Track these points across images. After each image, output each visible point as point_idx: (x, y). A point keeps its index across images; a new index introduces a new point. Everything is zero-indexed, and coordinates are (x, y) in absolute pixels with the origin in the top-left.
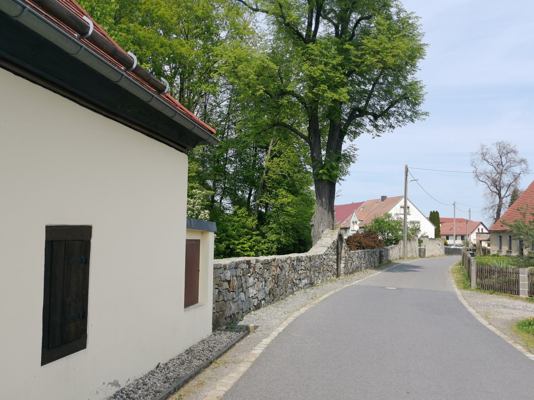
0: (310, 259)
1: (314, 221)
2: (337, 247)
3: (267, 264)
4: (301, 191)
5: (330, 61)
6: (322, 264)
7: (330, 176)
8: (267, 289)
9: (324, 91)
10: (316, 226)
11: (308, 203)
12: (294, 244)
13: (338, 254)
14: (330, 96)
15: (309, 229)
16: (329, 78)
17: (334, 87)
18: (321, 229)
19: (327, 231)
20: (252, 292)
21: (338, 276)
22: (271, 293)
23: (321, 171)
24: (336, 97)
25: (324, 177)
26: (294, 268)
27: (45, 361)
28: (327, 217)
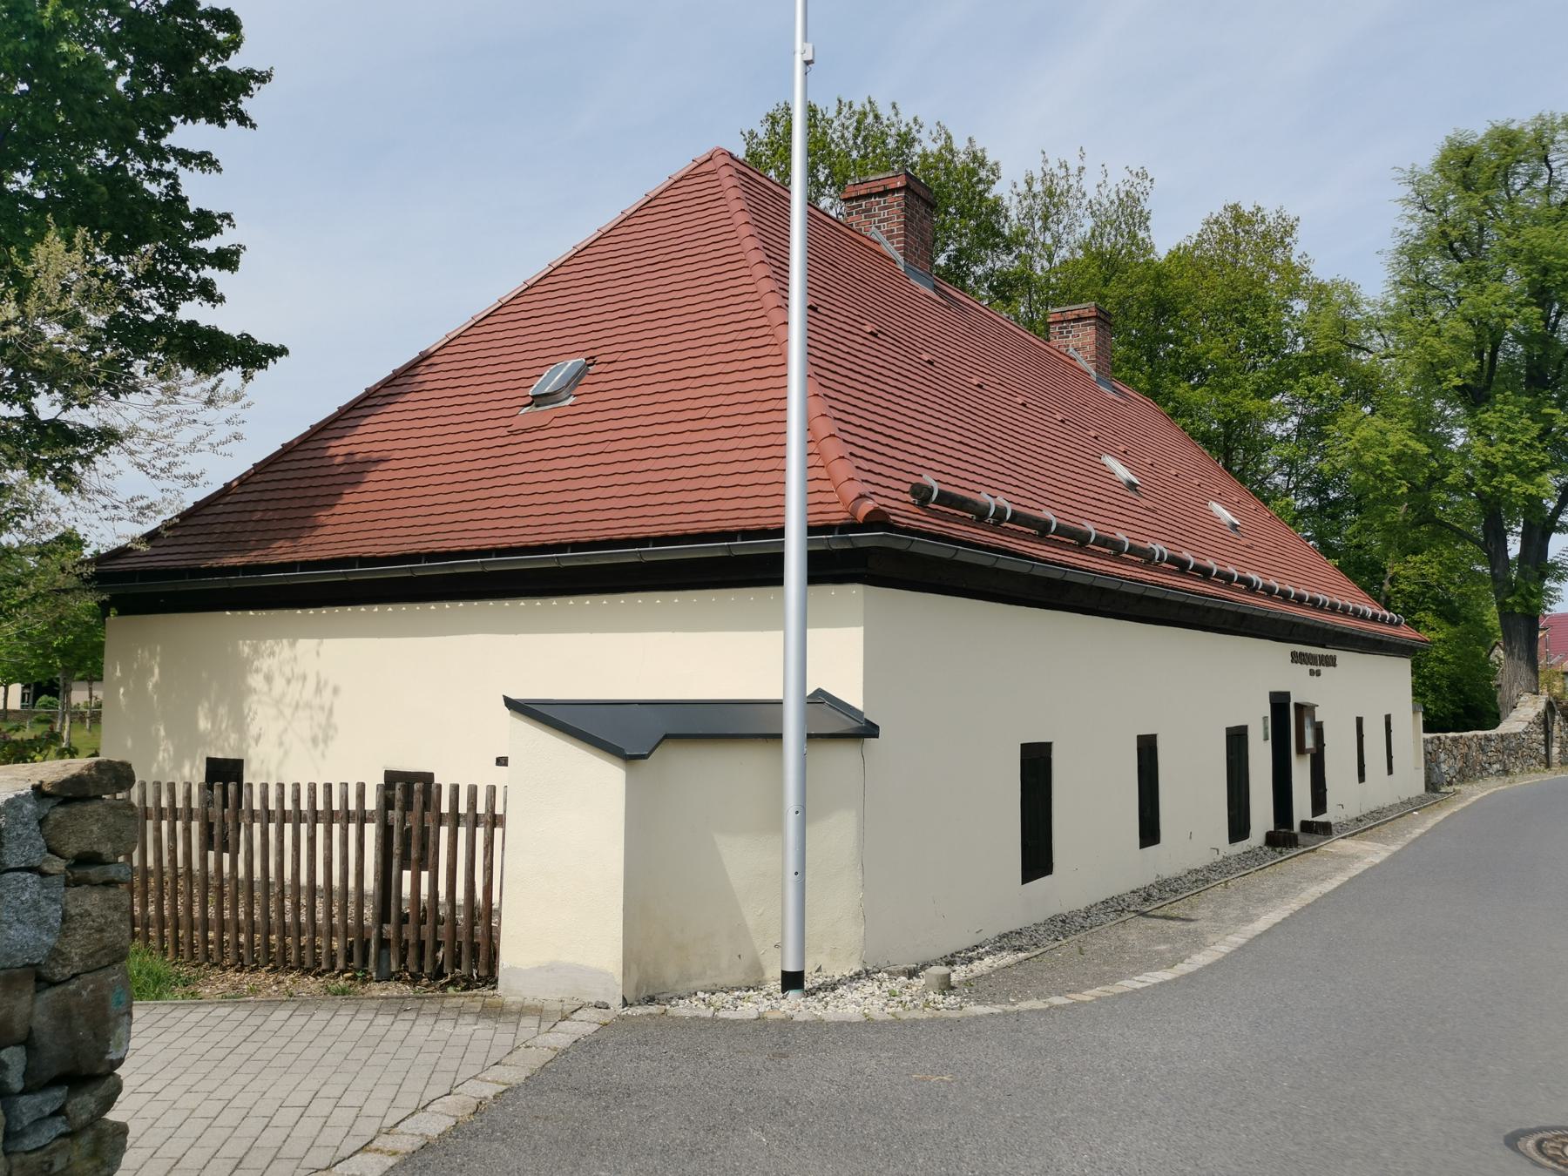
0: (1502, 738)
1: (1503, 678)
2: (1545, 722)
3: (1454, 740)
4: (1463, 611)
5: (1519, 436)
6: (1520, 746)
7: (1527, 607)
8: (1457, 767)
9: (1510, 484)
10: (1506, 688)
11: (1484, 639)
12: (1455, 715)
13: (1547, 732)
14: (1521, 491)
15: (1492, 697)
16: (1518, 464)
17: (1527, 475)
18: (1514, 693)
19: (1526, 697)
20: (1444, 767)
21: (1548, 766)
22: (1460, 771)
23: (1509, 600)
24: (1532, 490)
25: (1517, 610)
26: (1482, 749)
27: (1142, 846)
28: (1524, 670)
